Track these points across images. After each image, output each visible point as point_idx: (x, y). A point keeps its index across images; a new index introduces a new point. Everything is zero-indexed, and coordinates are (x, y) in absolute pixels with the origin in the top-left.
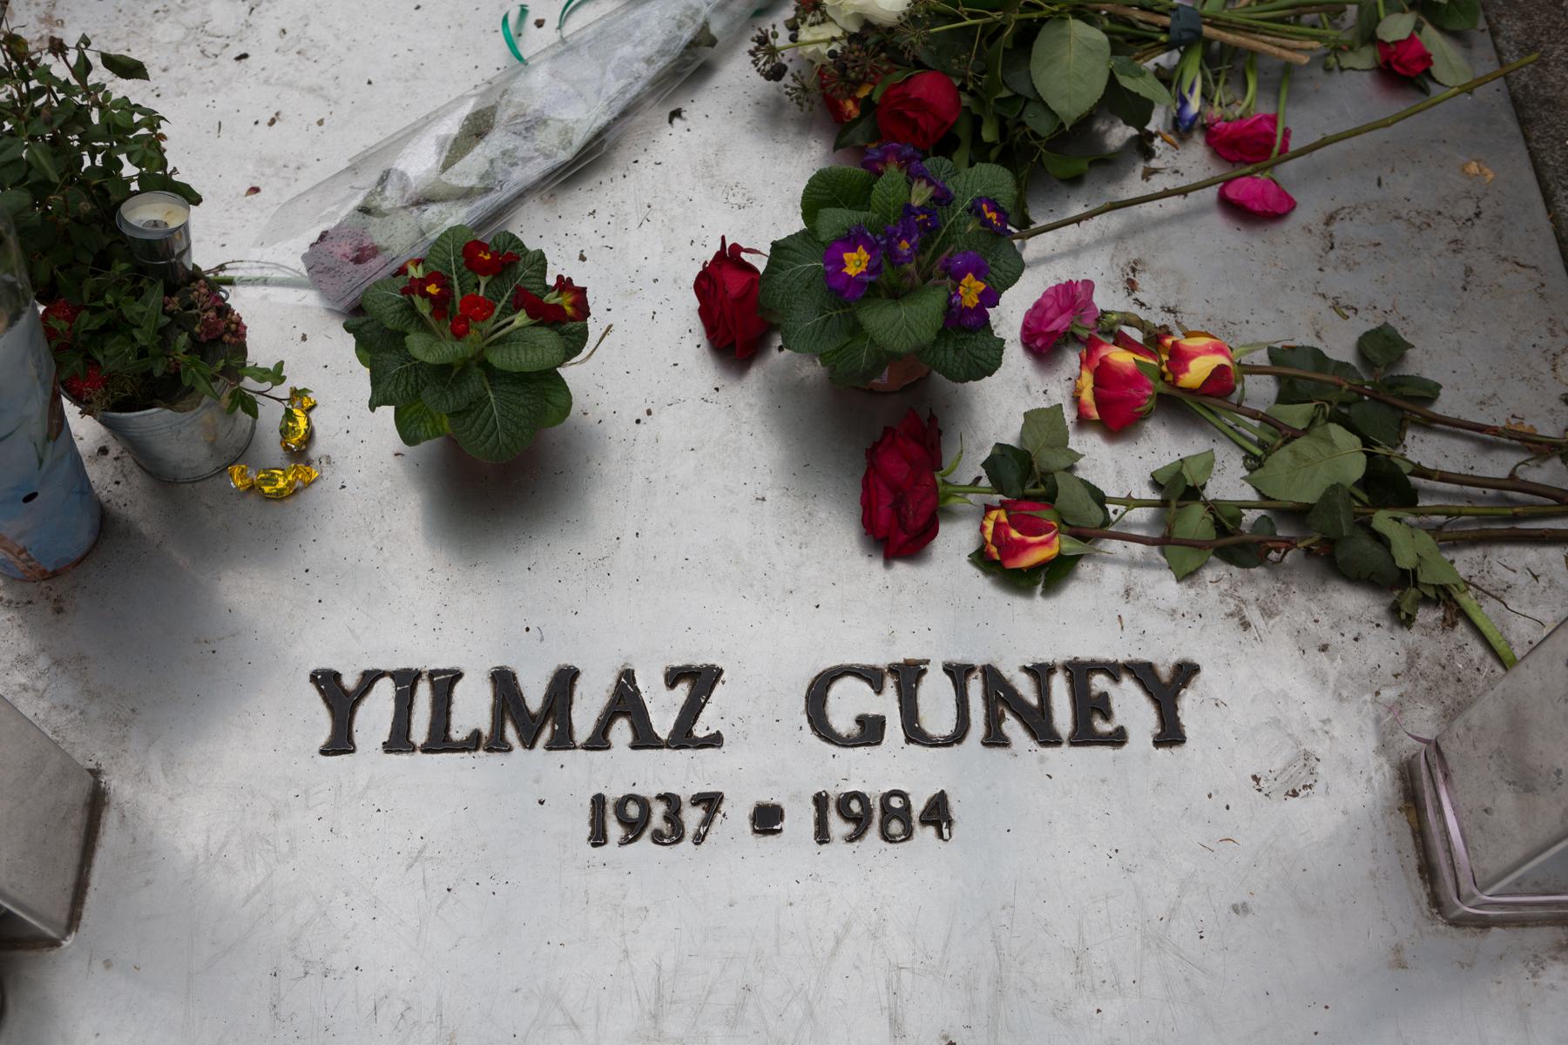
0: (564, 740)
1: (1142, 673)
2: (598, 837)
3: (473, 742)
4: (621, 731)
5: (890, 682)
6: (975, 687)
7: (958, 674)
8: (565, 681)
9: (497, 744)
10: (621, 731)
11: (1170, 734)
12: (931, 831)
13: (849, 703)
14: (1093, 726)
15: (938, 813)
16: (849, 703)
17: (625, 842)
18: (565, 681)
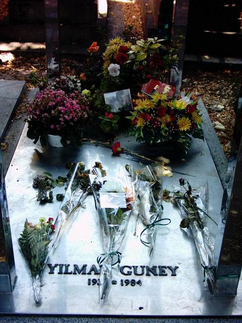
0: (84, 274)
1: (169, 268)
2: (89, 284)
3: (70, 273)
4: (93, 273)
5: (133, 268)
6: (145, 269)
7: (142, 267)
8: (85, 266)
9: (75, 274)
10: (93, 273)
11: (174, 275)
12: (138, 285)
13: (126, 270)
14: (163, 274)
15: (139, 282)
16: (126, 270)
17: (93, 285)
18: (85, 266)
